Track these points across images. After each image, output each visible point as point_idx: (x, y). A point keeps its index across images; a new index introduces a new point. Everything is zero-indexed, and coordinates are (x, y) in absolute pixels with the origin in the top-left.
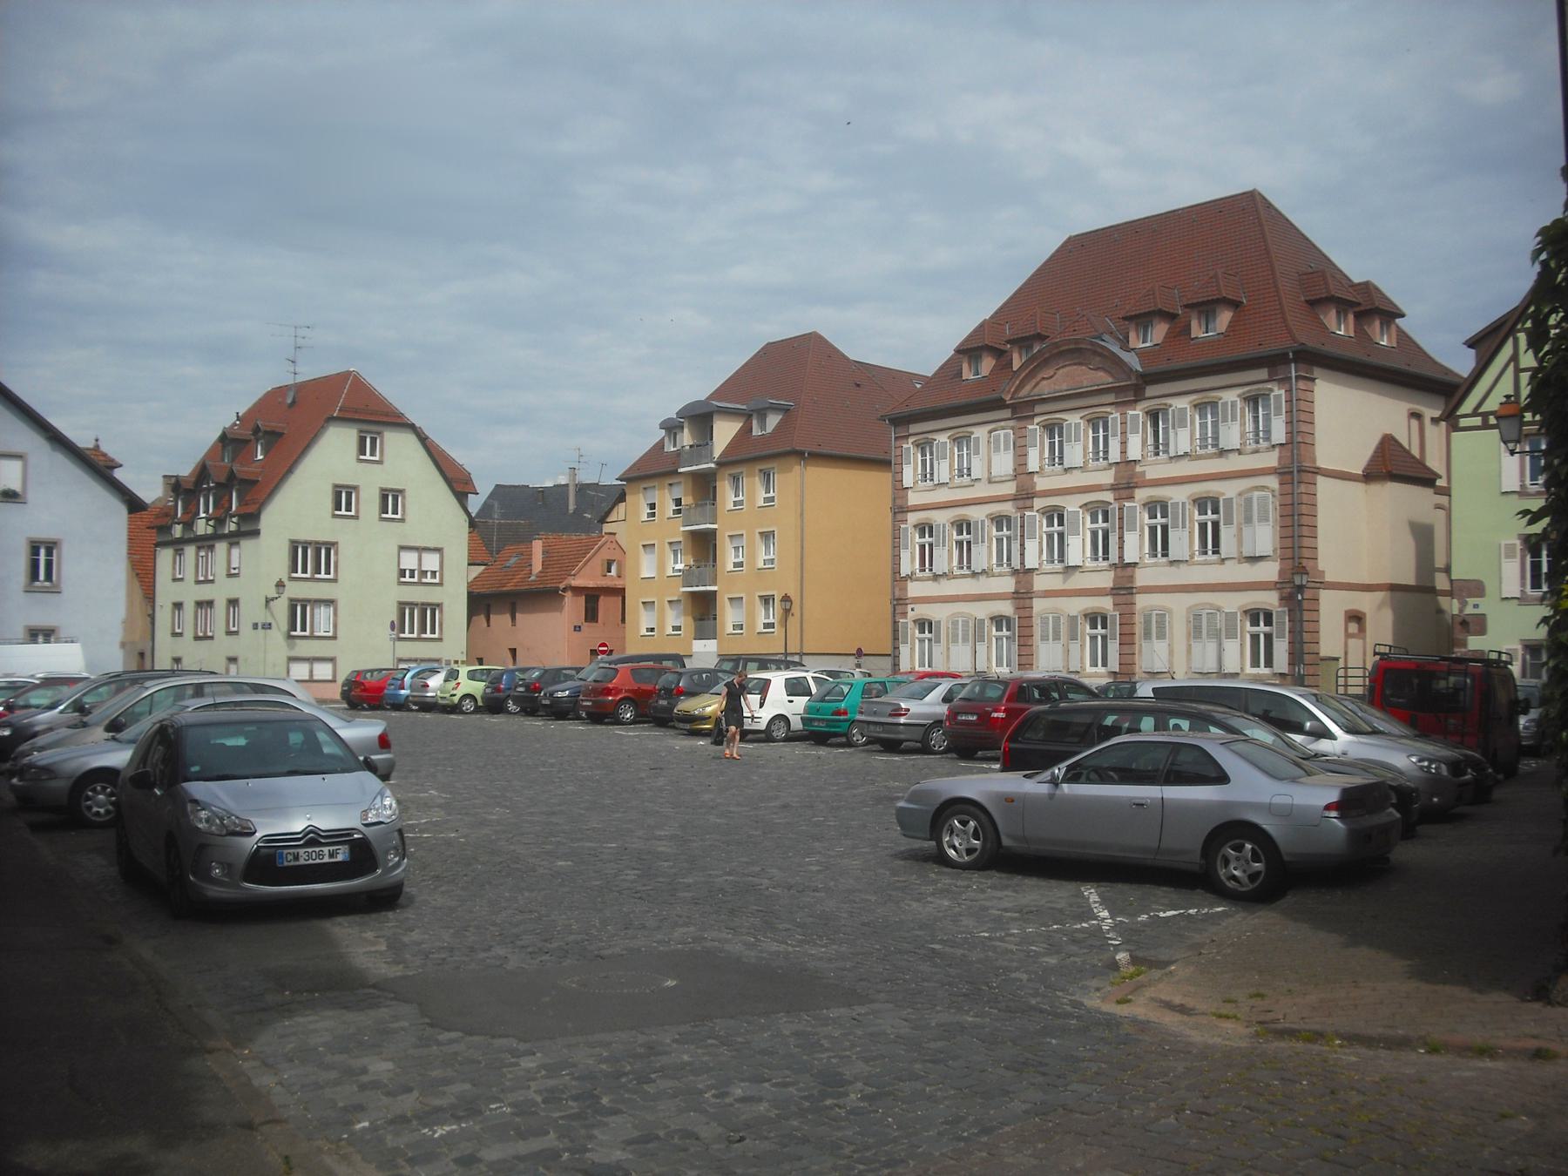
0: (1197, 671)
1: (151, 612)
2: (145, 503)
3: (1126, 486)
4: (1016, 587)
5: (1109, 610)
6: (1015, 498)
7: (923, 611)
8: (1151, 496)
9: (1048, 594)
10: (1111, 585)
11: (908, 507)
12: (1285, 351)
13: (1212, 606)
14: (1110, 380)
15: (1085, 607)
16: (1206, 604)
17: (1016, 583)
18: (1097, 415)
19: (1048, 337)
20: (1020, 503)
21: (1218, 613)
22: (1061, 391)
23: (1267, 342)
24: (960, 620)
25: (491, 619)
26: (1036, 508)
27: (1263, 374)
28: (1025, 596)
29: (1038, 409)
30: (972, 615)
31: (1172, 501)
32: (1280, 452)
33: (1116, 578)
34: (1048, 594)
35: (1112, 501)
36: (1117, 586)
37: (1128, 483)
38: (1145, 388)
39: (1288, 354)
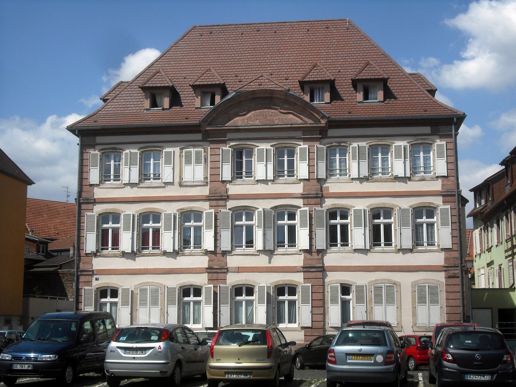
0: (334, 326)
1: (101, 256)
2: (212, 144)
3: (315, 195)
4: (209, 264)
5: (299, 282)
6: (207, 199)
7: (104, 281)
8: (335, 204)
9: (239, 270)
10: (207, 267)
11: (95, 199)
12: (452, 116)
13: (389, 281)
14: (313, 122)
15: (279, 279)
16: (385, 279)
17: (209, 261)
18: (284, 145)
19: (427, 90)
20: (214, 203)
21: (395, 286)
22: (254, 126)
23: (429, 110)
24: (427, 285)
25: (320, 273)
26: (227, 209)
27: (427, 130)
28: (219, 271)
29: (229, 136)
30: (161, 284)
31: (354, 209)
32: (442, 182)
33: (305, 259)
34: (239, 270)
35: (302, 206)
36: (307, 266)
37: (317, 194)
38: (327, 131)
39: (453, 119)
